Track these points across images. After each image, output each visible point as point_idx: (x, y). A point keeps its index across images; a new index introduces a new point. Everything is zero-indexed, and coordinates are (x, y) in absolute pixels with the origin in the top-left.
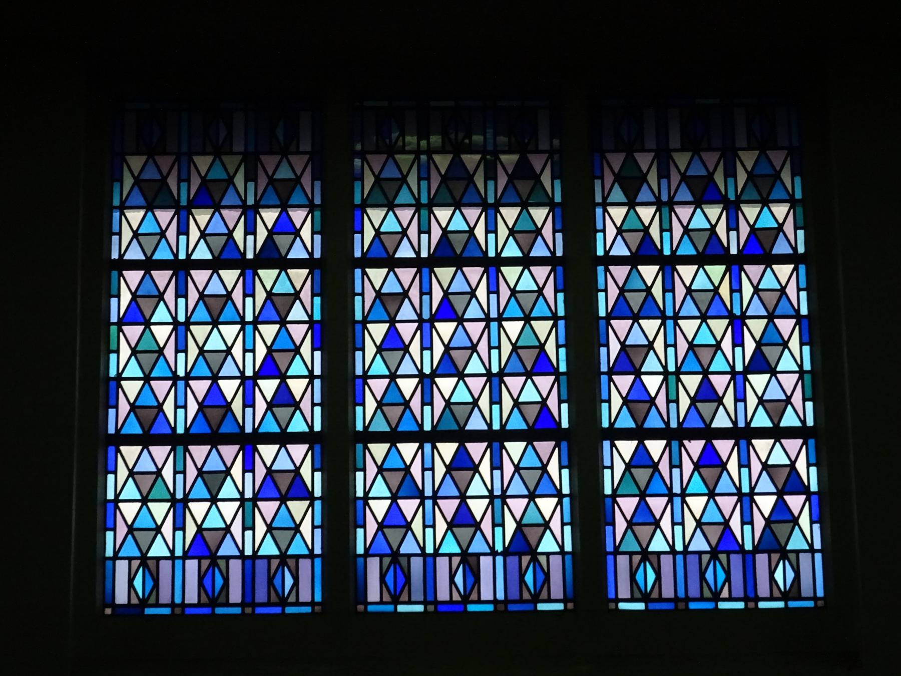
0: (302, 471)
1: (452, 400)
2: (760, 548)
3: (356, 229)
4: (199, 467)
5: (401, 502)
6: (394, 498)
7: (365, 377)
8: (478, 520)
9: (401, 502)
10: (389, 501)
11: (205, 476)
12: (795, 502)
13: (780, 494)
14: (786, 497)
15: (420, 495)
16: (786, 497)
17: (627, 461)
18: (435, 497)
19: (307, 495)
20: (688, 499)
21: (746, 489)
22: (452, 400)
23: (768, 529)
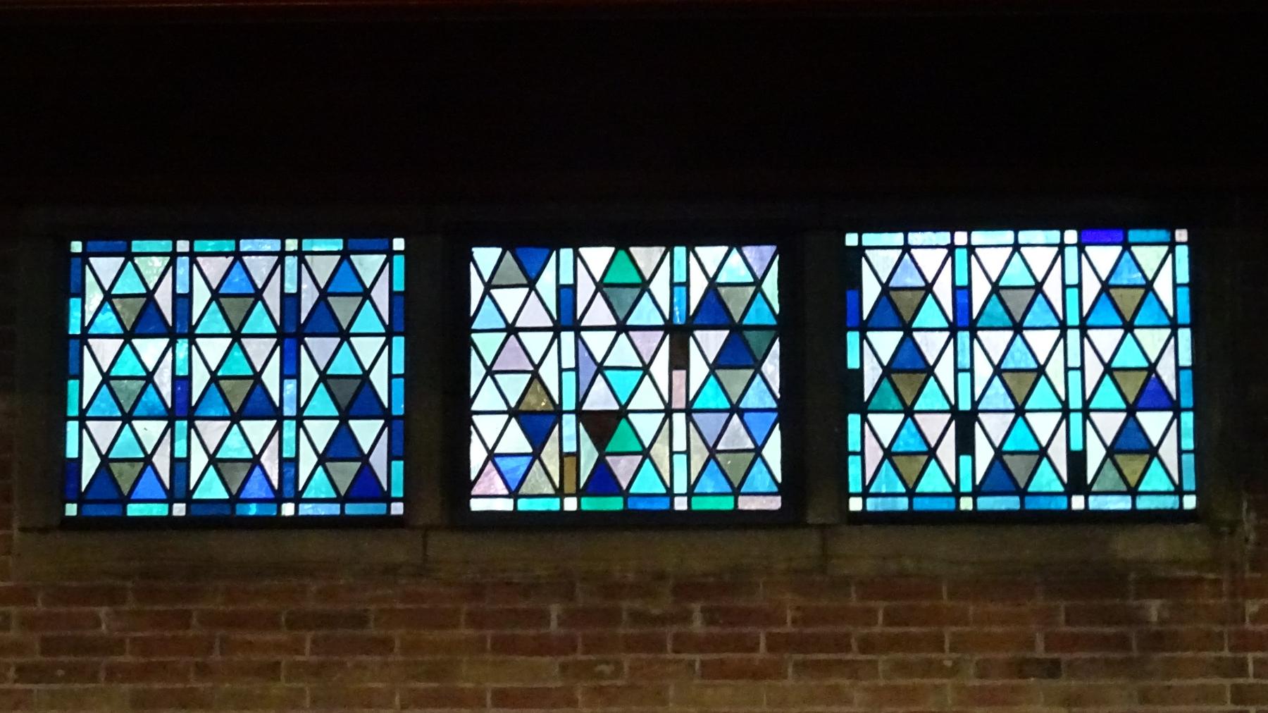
0: (372, 376)
1: (1002, 283)
2: (984, 489)
3: (73, 290)
4: (322, 368)
5: (1141, 416)
6: (1131, 410)
7: (85, 336)
8: (366, 451)
9: (1141, 416)
10: (336, 422)
11: (330, 381)
12: (1154, 423)
13: (344, 417)
14: (352, 423)
15: (276, 413)
16: (352, 423)
17: (885, 363)
18: (668, 412)
19: (379, 412)
20: (89, 424)
21: (965, 405)
22: (1002, 283)
23: (997, 463)
